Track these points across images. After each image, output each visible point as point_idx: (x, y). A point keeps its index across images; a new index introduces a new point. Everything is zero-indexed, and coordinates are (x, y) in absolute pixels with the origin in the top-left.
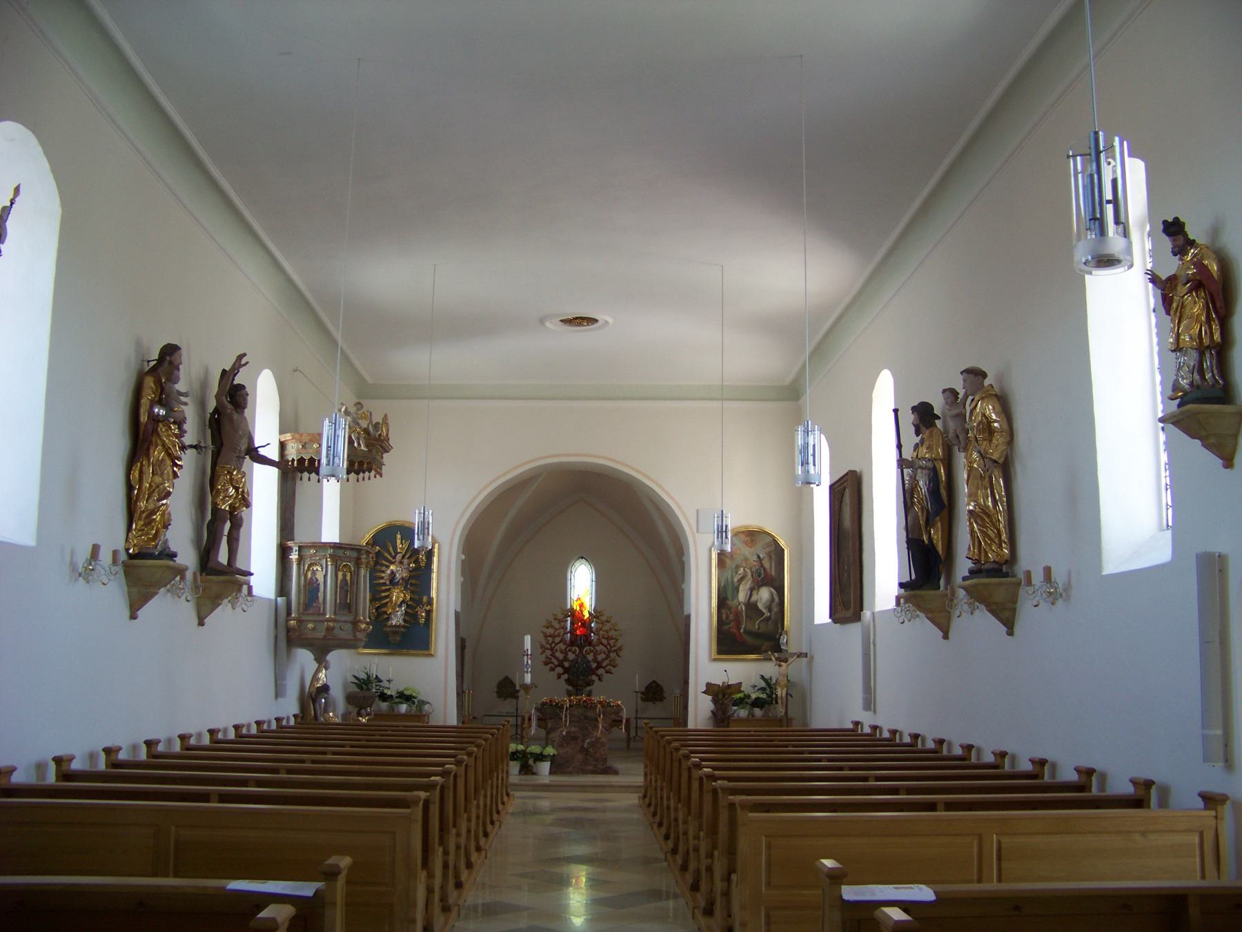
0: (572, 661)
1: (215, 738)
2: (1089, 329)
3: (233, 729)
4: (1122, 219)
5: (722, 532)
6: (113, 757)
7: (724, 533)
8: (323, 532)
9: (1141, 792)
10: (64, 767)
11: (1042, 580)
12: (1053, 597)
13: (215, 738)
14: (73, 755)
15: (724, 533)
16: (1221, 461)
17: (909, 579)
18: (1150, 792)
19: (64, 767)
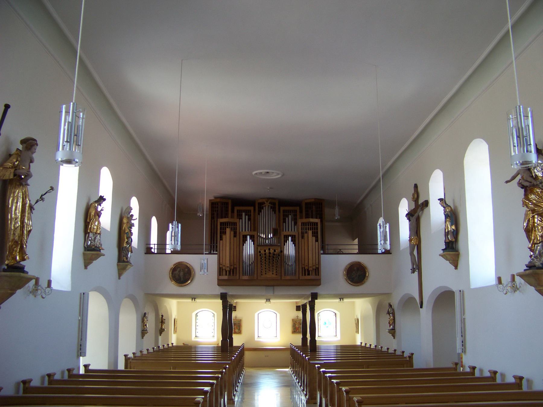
0: (142, 355)
1: (87, 369)
2: (465, 179)
3: (67, 371)
4: (386, 319)
5: (175, 236)
6: (27, 385)
7: (173, 235)
8: (418, 296)
9: (493, 375)
10: (51, 378)
11: (510, 281)
12: (34, 292)
13: (87, 369)
14: (31, 379)
15: (173, 235)
16: (454, 267)
17: (358, 245)
18: (496, 375)
19: (51, 378)
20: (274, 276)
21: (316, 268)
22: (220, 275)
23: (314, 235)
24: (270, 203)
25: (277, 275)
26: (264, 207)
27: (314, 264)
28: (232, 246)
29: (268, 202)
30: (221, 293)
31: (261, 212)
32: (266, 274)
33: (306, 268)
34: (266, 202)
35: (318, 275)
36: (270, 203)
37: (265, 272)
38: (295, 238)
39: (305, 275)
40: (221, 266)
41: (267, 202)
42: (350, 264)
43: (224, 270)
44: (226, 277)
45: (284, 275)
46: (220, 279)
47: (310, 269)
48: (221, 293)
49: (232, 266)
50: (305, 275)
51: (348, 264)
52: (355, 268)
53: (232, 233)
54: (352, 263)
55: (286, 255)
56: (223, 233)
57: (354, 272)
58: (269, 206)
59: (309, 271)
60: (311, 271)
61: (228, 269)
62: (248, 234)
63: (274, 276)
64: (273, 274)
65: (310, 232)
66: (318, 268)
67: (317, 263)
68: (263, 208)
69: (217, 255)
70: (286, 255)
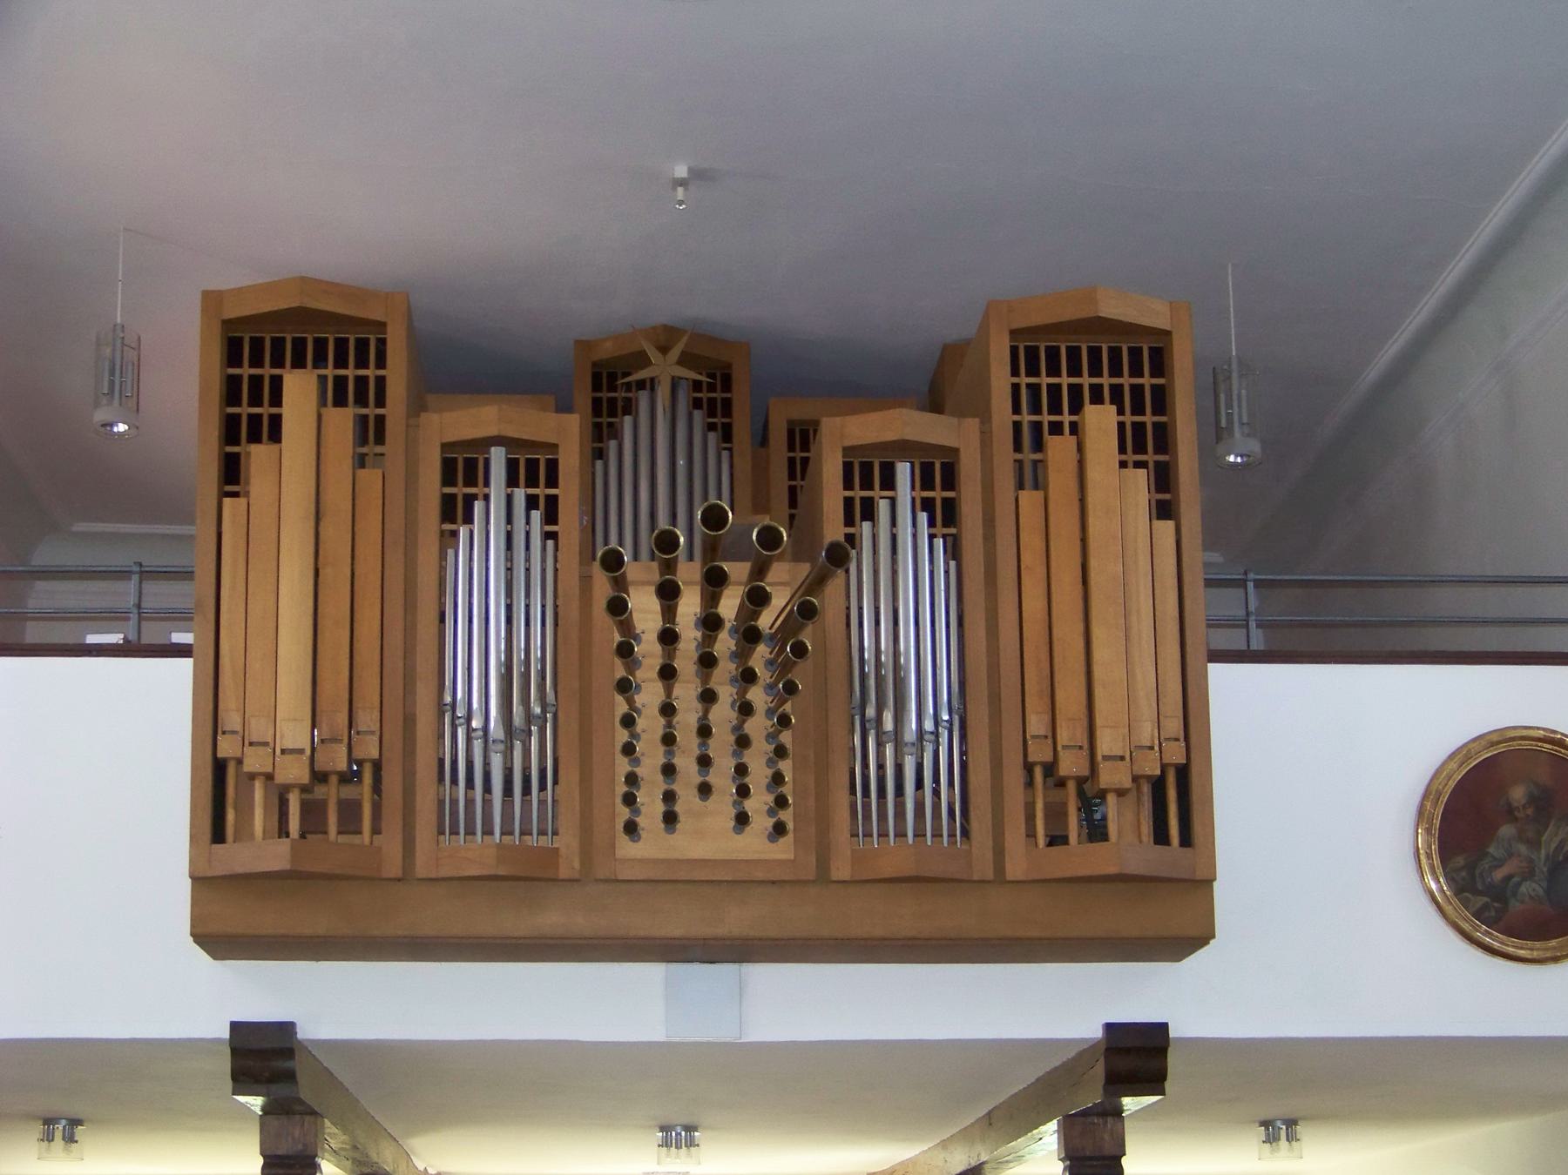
20: (754, 844)
21: (1164, 767)
22: (218, 836)
23: (1131, 457)
24: (681, 362)
25: (779, 829)
26: (643, 398)
27: (1146, 733)
28: (334, 578)
29: (675, 353)
30: (235, 1026)
31: (615, 433)
32: (670, 819)
33: (1071, 765)
34: (654, 355)
35: (1186, 840)
36: (681, 362)
37: (660, 808)
38: (950, 481)
39: (1057, 840)
40: (227, 748)
41: (664, 350)
42: (1493, 744)
43: (258, 787)
44: (275, 856)
45: (854, 835)
46: (219, 870)
47: (1117, 776)
48: (235, 1026)
49: (341, 741)
50: (1057, 840)
51: (1452, 756)
52: (1518, 794)
53: (342, 421)
54: (1501, 737)
55: (870, 668)
56: (255, 438)
57: (1506, 831)
58: (675, 383)
59: (1090, 798)
60: (1121, 793)
61: (294, 772)
62: (492, 431)
63: (754, 844)
64: (742, 819)
65: (1101, 421)
66: (1183, 772)
67: (1174, 726)
68: (629, 408)
69: (186, 664)
70: (870, 668)
